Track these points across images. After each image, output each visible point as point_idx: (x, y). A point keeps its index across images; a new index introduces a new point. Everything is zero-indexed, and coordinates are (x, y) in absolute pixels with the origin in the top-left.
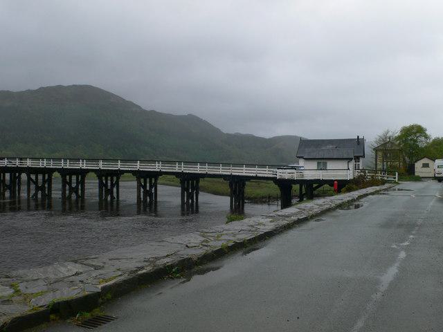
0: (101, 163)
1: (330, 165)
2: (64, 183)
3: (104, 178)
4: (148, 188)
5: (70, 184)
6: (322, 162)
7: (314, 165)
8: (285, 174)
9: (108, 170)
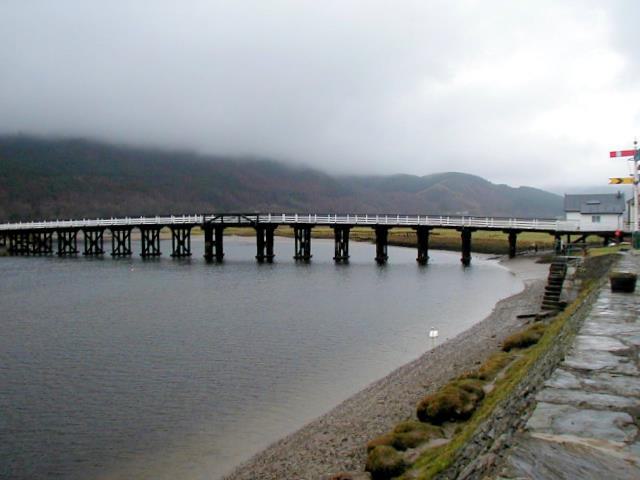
0: (377, 218)
1: (604, 219)
6: (596, 216)
7: (589, 219)
8: (557, 226)
9: (24, 221)
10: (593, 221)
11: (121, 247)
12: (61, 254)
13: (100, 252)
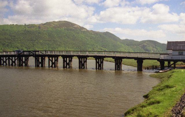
2: (64, 61)
3: (65, 59)
4: (83, 63)
5: (66, 61)
10: (170, 12)
11: (14, 60)
12: (20, 65)
13: (22, 65)
